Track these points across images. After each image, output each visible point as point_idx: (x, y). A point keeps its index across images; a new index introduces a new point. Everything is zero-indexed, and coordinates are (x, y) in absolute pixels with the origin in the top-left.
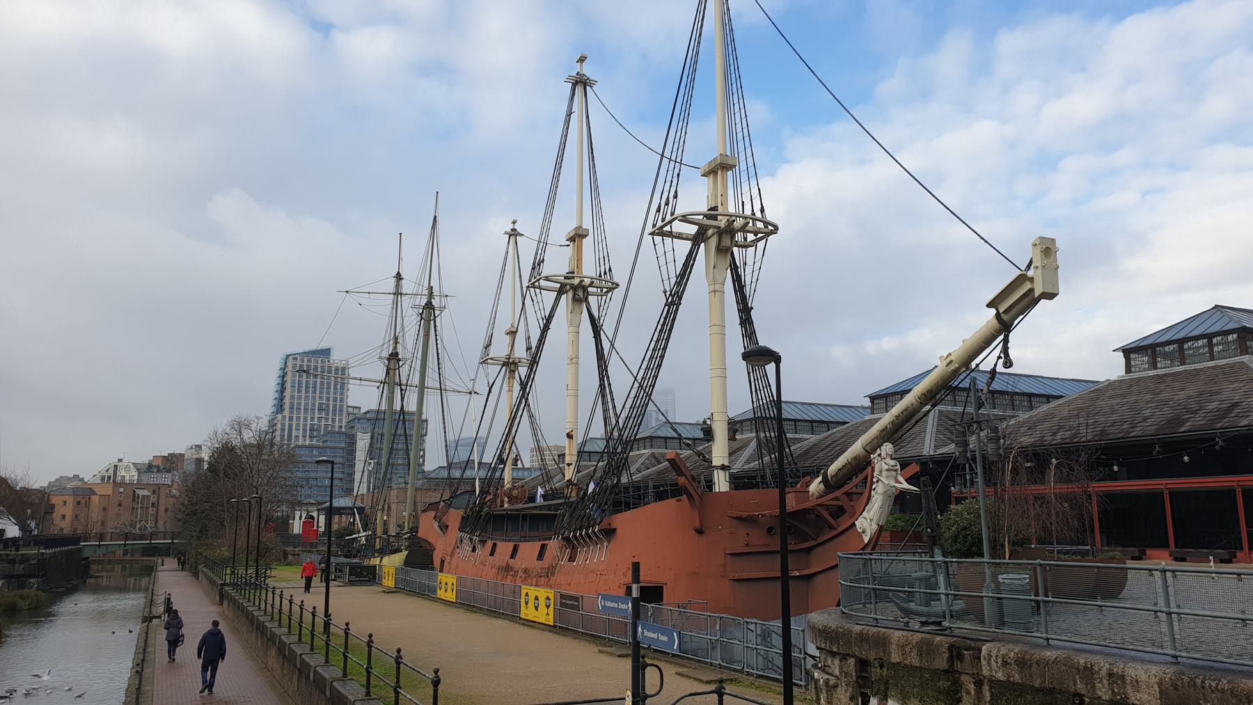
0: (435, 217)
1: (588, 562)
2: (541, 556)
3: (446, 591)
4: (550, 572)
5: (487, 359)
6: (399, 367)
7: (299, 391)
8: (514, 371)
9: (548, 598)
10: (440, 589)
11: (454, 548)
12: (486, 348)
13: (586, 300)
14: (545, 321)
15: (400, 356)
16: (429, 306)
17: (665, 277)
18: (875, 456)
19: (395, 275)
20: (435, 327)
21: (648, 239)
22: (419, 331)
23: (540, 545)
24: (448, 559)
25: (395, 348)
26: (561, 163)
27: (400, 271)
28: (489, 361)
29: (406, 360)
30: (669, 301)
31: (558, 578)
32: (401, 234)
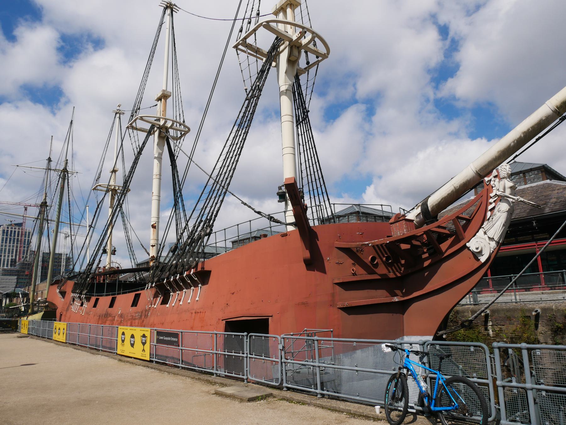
0: (72, 121)
1: (181, 303)
2: (135, 303)
3: (59, 334)
4: (145, 314)
5: (97, 186)
7: (6, 243)
9: (144, 336)
10: (55, 333)
11: (69, 305)
14: (138, 149)
15: (48, 204)
16: (65, 171)
19: (47, 158)
20: (68, 183)
21: (231, 51)
22: (58, 184)
24: (64, 313)
25: (45, 199)
26: (156, 44)
28: (99, 188)
31: (152, 319)
32: (52, 136)
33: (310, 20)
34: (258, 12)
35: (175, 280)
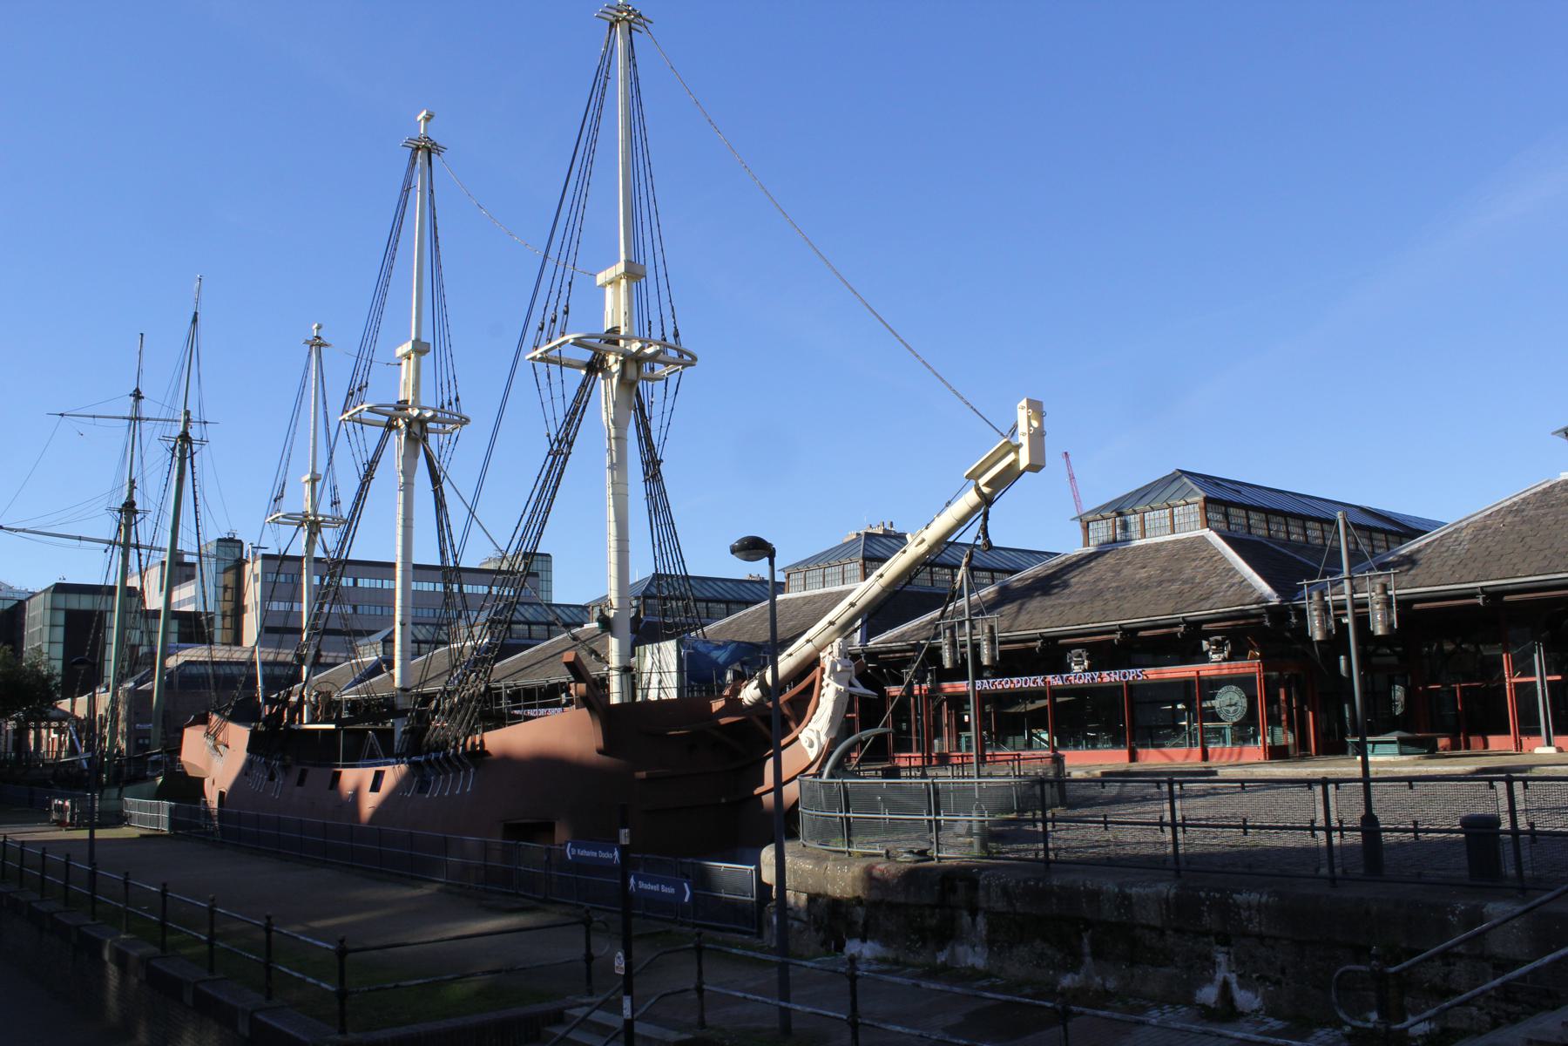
0: (196, 314)
6: (136, 523)
8: (315, 534)
12: (275, 501)
13: (425, 439)
14: (366, 466)
15: (137, 507)
16: (185, 437)
17: (550, 417)
18: (825, 654)
23: (374, 772)
25: (131, 494)
27: (140, 387)
29: (145, 512)
30: (555, 448)
32: (142, 334)
33: (668, 287)
34: (565, 309)
35: (437, 759)
